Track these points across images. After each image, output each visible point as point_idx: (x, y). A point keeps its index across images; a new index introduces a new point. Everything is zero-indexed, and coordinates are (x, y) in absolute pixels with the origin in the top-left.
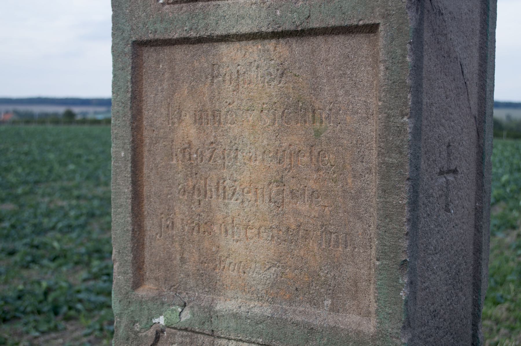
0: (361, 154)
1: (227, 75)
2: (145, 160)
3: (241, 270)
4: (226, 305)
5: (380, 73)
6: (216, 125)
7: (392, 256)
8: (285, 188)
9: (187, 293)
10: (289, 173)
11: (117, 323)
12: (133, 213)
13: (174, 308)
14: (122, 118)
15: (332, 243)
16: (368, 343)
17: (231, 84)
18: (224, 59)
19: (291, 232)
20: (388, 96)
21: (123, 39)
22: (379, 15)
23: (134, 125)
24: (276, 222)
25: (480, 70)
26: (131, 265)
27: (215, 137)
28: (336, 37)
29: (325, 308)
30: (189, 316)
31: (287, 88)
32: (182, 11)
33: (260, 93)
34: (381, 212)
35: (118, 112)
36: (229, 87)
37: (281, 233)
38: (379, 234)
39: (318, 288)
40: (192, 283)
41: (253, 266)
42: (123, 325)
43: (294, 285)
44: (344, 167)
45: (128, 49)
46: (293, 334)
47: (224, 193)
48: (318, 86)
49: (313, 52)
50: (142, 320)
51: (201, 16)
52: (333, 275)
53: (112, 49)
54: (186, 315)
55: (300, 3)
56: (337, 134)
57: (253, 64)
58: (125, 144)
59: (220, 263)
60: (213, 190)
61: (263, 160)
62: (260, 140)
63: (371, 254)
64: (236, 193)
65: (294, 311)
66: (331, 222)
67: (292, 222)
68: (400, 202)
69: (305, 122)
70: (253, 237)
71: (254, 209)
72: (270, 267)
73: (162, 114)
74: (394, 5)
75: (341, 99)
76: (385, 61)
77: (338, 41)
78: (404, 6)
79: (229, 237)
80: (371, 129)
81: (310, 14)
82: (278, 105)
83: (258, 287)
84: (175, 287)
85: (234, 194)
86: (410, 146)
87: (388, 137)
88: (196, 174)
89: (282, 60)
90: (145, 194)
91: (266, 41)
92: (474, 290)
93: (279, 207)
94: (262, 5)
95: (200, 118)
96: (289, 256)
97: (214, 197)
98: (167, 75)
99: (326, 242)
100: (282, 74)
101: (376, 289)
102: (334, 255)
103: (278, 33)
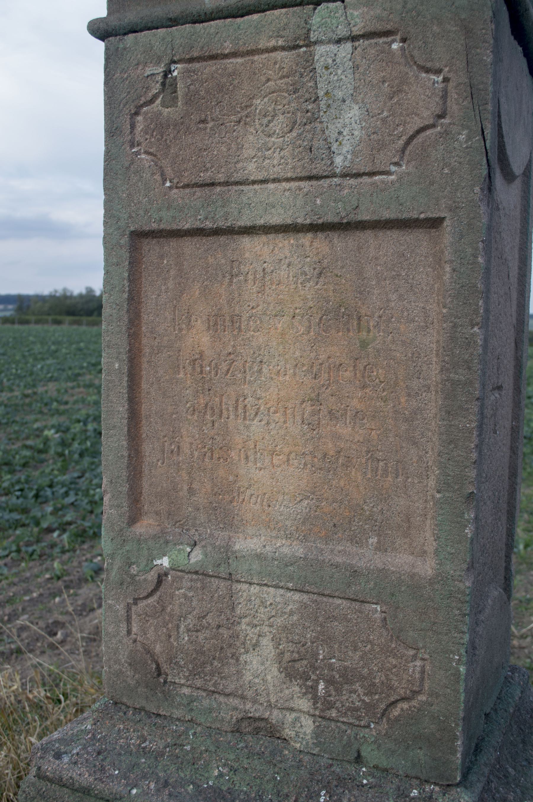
0: (417, 369)
1: (250, 273)
2: (144, 372)
3: (264, 503)
4: (247, 543)
5: (445, 276)
6: (235, 333)
7: (456, 487)
8: (322, 407)
9: (196, 530)
10: (327, 391)
11: (108, 564)
12: (129, 435)
13: (181, 547)
14: (117, 322)
15: (380, 472)
16: (425, 587)
17: (255, 284)
18: (247, 255)
19: (328, 458)
20: (455, 302)
21: (119, 228)
22: (446, 207)
23: (132, 331)
24: (310, 448)
25: (519, 274)
26: (127, 497)
27: (234, 346)
28: (388, 232)
29: (370, 547)
30: (200, 557)
31: (326, 290)
32: (195, 197)
33: (292, 296)
34: (444, 437)
35: (111, 315)
36: (252, 288)
37: (316, 460)
38: (441, 462)
39: (361, 523)
40: (202, 518)
41: (280, 498)
42: (116, 567)
43: (332, 520)
44: (396, 384)
45: (125, 240)
46: (331, 578)
47: (245, 412)
48: (365, 289)
49: (359, 248)
50: (139, 561)
51: (220, 203)
52: (380, 509)
53: (104, 240)
54: (197, 556)
55: (346, 191)
56: (388, 345)
57: (283, 262)
58: (119, 353)
59: (239, 495)
60: (231, 409)
61: (295, 374)
62: (291, 351)
63: (427, 485)
64: (259, 413)
65: (332, 551)
66: (379, 447)
67: (330, 447)
68: (468, 425)
69: (348, 330)
70: (280, 465)
71: (282, 432)
72: (302, 500)
73: (166, 318)
74: (464, 196)
75: (393, 304)
76: (451, 262)
77: (391, 236)
78: (476, 198)
79: (250, 464)
80: (431, 341)
81: (358, 204)
82: (314, 310)
83: (286, 523)
84: (182, 522)
85: (257, 414)
86: (481, 361)
87: (455, 350)
88: (209, 390)
89: (320, 257)
90: (143, 413)
91: (301, 235)
92: (508, 518)
93: (314, 430)
94: (297, 192)
95: (216, 323)
96: (326, 487)
97: (232, 417)
98: (172, 273)
99: (372, 470)
100: (320, 274)
101: (436, 525)
102: (382, 486)
103: (317, 225)
